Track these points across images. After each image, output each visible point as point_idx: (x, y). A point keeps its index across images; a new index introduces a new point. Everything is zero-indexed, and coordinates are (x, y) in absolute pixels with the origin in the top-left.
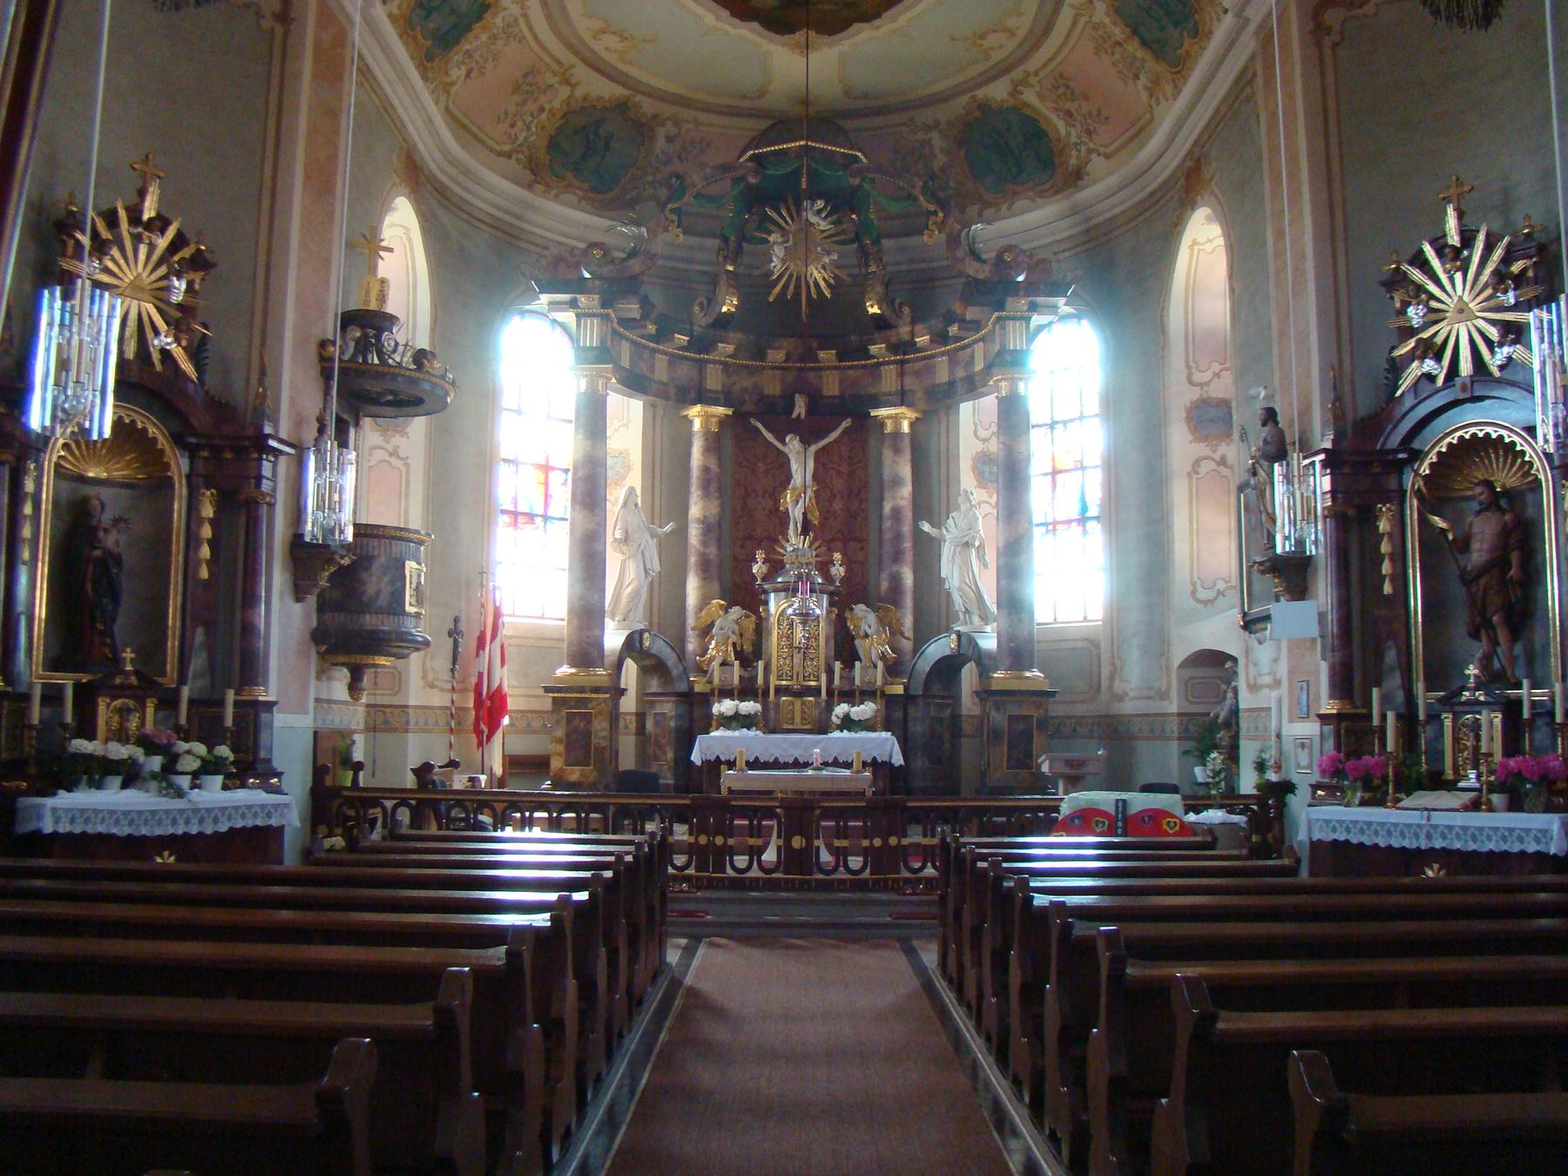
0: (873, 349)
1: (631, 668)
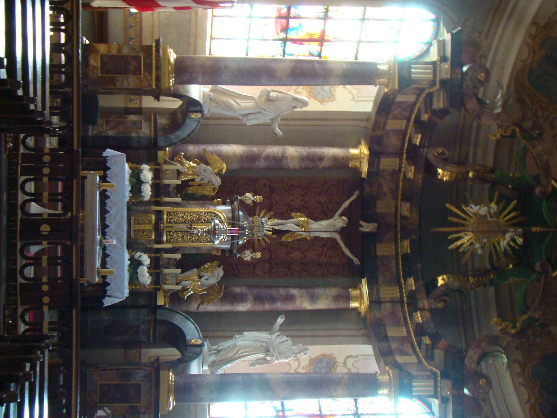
0: (411, 281)
1: (175, 104)
